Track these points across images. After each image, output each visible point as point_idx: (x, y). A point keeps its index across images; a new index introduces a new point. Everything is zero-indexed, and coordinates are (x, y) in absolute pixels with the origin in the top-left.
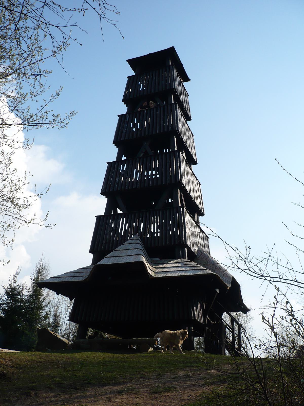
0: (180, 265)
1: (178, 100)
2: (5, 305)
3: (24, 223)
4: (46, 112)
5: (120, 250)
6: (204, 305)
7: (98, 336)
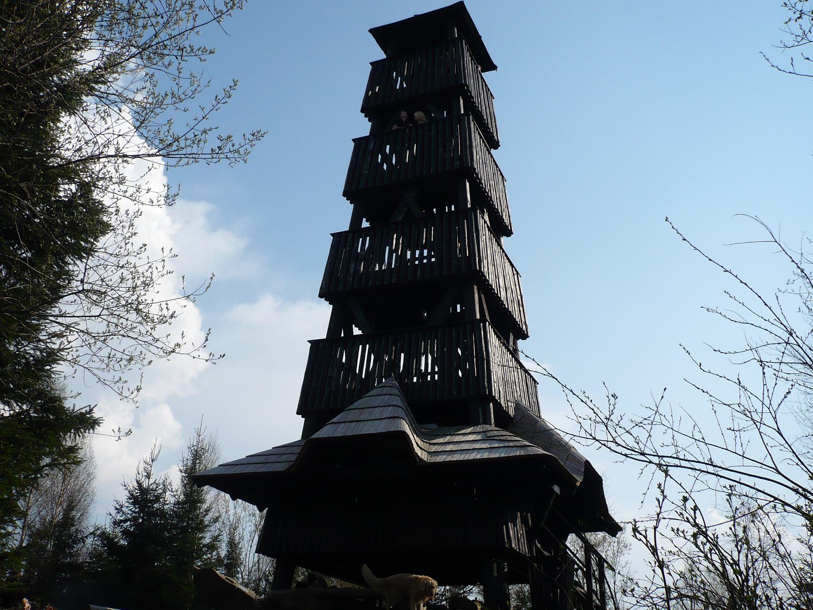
0: (479, 437)
1: (472, 108)
2: (128, 523)
3: (161, 353)
4: (205, 132)
5: (358, 409)
6: (530, 518)
7: (316, 582)
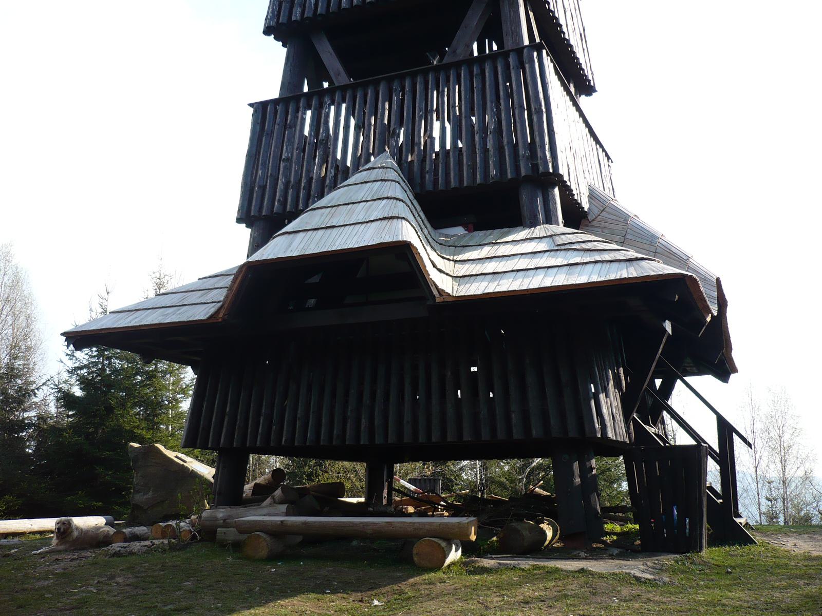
0: (542, 246)
2: (85, 370)
